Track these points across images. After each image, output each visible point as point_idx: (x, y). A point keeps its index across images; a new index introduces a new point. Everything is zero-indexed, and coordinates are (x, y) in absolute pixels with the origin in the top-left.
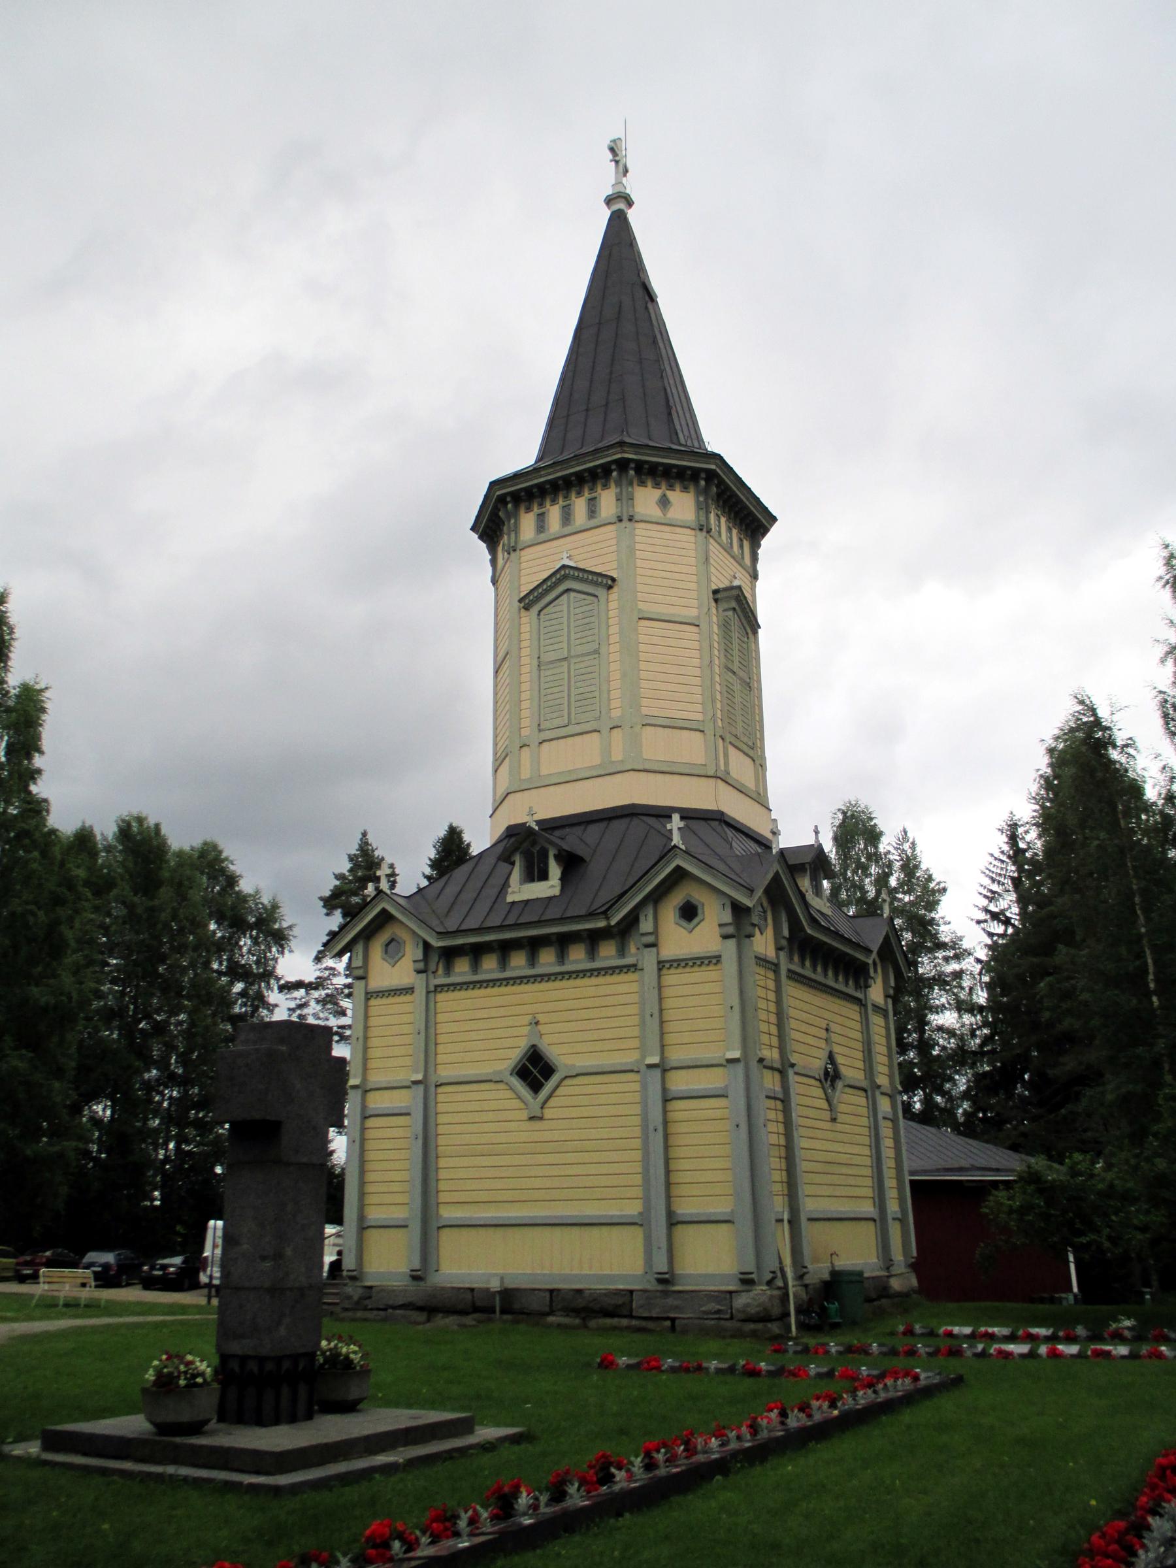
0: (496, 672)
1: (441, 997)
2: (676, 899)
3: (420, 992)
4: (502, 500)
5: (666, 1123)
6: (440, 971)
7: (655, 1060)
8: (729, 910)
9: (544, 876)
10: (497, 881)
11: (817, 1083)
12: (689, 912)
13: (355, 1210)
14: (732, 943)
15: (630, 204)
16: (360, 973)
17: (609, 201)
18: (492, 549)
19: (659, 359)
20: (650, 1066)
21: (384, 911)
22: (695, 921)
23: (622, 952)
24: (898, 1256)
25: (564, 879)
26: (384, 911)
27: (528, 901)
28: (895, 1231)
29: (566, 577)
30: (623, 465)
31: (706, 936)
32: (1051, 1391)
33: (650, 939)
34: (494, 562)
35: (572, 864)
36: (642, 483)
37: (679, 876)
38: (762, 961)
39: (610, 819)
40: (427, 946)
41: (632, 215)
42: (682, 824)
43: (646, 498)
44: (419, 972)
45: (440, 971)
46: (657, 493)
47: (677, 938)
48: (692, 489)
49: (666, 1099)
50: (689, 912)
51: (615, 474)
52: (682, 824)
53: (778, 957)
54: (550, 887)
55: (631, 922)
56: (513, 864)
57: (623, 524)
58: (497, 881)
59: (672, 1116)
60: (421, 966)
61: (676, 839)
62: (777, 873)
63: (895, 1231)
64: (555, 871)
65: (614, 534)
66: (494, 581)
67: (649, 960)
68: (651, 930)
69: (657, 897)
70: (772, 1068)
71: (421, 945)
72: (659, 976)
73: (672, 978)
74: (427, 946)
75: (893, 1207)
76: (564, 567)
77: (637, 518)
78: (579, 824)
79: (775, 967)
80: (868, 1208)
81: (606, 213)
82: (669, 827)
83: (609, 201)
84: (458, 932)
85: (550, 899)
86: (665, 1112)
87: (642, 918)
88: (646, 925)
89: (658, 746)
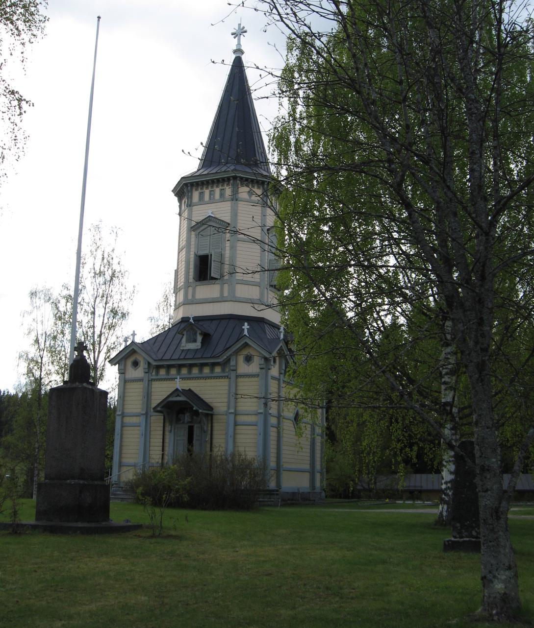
0: (179, 253)
1: (153, 383)
2: (245, 352)
3: (146, 380)
4: (186, 185)
5: (235, 434)
6: (154, 373)
7: (232, 411)
8: (263, 359)
9: (195, 341)
10: (176, 342)
11: (291, 422)
12: (248, 359)
13: (118, 460)
14: (263, 371)
15: (242, 53)
16: (123, 371)
17: (235, 52)
18: (180, 201)
19: (250, 123)
20: (230, 413)
21: (133, 349)
22: (250, 362)
23: (223, 370)
24: (318, 484)
25: (203, 343)
26: (133, 349)
27: (189, 350)
28: (318, 477)
29: (210, 220)
30: (235, 178)
31: (254, 367)
32: (396, 550)
33: (234, 368)
34: (180, 207)
35: (206, 337)
36: (242, 185)
37: (246, 345)
38: (273, 378)
39: (221, 319)
40: (149, 363)
41: (244, 58)
42: (248, 327)
43: (243, 191)
44: (146, 373)
45: (154, 373)
46: (247, 189)
47: (243, 368)
48: (261, 187)
49: (236, 424)
50: (248, 359)
51: (231, 181)
52: (248, 327)
53: (280, 376)
54: (197, 345)
55: (228, 360)
56: (183, 335)
57: (233, 202)
58: (176, 342)
59: (238, 431)
60: (147, 371)
61: (246, 333)
62: (281, 346)
63: (318, 477)
64: (199, 338)
65: (230, 205)
66: (180, 214)
67: (233, 375)
68: (235, 364)
69: (237, 352)
70: (274, 416)
71: (147, 363)
72: (236, 380)
73: (240, 380)
74: (149, 363)
75: (318, 467)
76: (210, 216)
77: (239, 199)
78: (208, 320)
79: (279, 380)
80: (307, 467)
81: (234, 56)
82: (243, 327)
83: (235, 52)
84: (161, 360)
85: (197, 349)
86: (235, 429)
87: (231, 360)
88: (232, 363)
89: (242, 291)
